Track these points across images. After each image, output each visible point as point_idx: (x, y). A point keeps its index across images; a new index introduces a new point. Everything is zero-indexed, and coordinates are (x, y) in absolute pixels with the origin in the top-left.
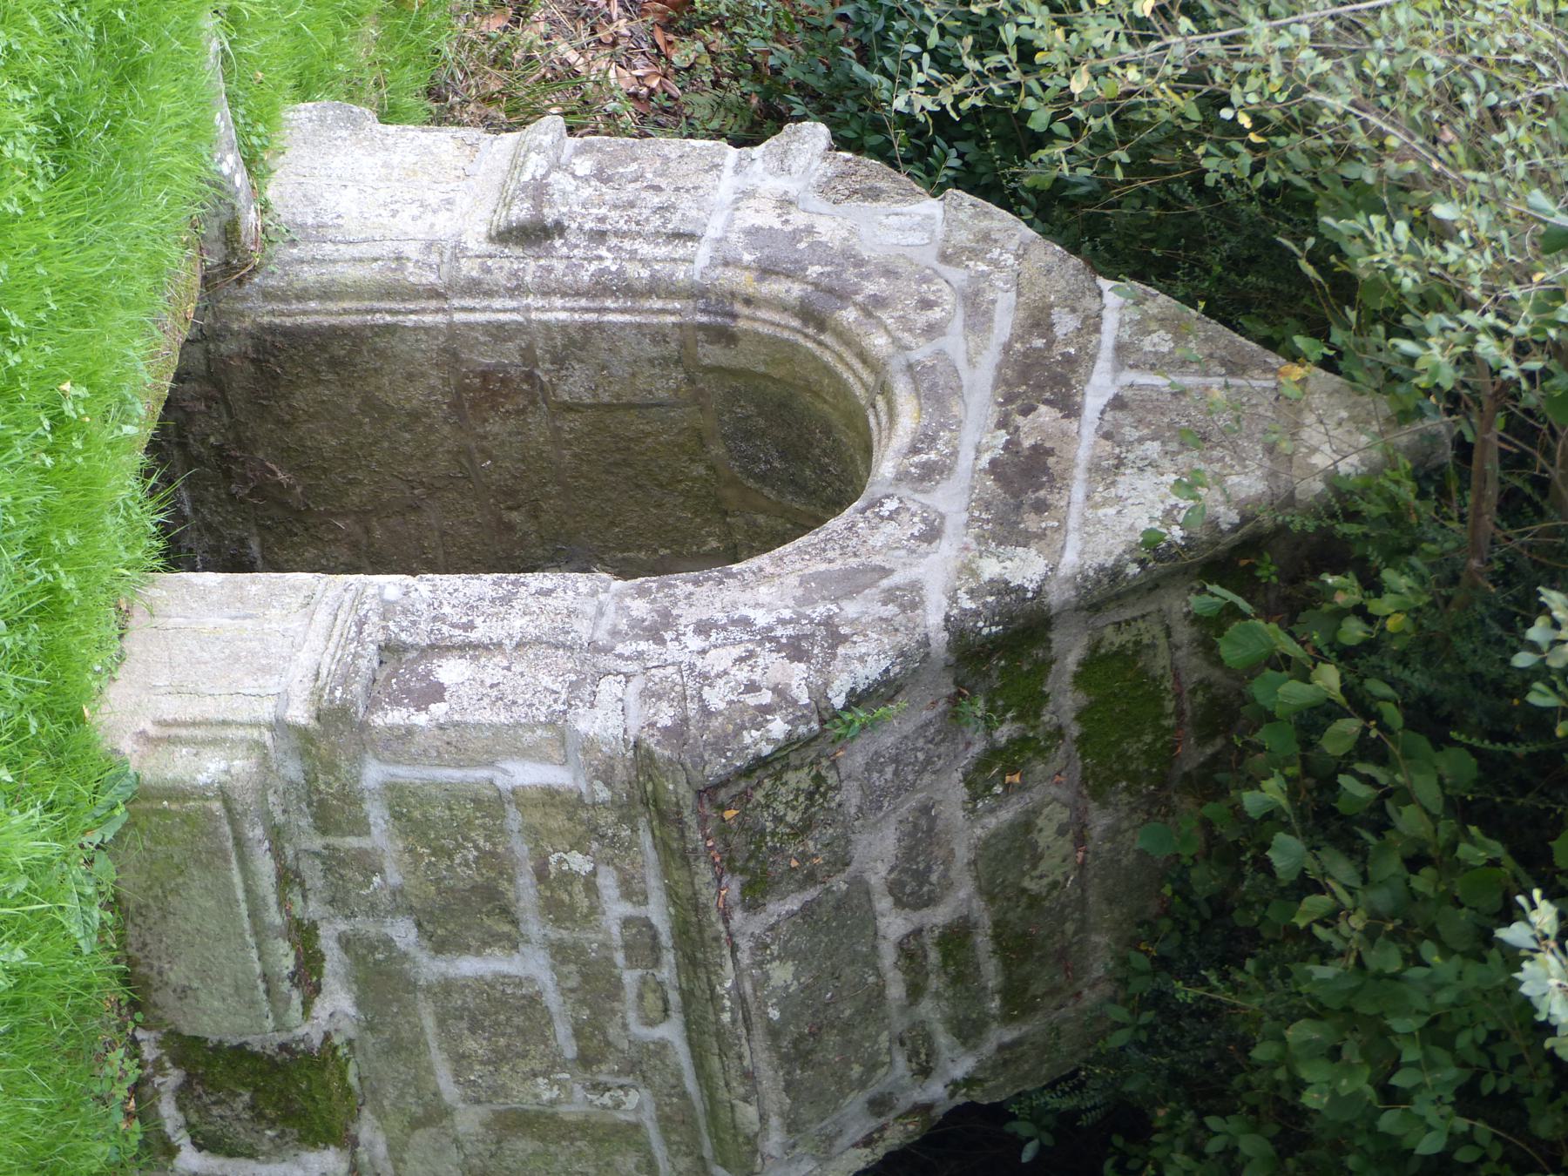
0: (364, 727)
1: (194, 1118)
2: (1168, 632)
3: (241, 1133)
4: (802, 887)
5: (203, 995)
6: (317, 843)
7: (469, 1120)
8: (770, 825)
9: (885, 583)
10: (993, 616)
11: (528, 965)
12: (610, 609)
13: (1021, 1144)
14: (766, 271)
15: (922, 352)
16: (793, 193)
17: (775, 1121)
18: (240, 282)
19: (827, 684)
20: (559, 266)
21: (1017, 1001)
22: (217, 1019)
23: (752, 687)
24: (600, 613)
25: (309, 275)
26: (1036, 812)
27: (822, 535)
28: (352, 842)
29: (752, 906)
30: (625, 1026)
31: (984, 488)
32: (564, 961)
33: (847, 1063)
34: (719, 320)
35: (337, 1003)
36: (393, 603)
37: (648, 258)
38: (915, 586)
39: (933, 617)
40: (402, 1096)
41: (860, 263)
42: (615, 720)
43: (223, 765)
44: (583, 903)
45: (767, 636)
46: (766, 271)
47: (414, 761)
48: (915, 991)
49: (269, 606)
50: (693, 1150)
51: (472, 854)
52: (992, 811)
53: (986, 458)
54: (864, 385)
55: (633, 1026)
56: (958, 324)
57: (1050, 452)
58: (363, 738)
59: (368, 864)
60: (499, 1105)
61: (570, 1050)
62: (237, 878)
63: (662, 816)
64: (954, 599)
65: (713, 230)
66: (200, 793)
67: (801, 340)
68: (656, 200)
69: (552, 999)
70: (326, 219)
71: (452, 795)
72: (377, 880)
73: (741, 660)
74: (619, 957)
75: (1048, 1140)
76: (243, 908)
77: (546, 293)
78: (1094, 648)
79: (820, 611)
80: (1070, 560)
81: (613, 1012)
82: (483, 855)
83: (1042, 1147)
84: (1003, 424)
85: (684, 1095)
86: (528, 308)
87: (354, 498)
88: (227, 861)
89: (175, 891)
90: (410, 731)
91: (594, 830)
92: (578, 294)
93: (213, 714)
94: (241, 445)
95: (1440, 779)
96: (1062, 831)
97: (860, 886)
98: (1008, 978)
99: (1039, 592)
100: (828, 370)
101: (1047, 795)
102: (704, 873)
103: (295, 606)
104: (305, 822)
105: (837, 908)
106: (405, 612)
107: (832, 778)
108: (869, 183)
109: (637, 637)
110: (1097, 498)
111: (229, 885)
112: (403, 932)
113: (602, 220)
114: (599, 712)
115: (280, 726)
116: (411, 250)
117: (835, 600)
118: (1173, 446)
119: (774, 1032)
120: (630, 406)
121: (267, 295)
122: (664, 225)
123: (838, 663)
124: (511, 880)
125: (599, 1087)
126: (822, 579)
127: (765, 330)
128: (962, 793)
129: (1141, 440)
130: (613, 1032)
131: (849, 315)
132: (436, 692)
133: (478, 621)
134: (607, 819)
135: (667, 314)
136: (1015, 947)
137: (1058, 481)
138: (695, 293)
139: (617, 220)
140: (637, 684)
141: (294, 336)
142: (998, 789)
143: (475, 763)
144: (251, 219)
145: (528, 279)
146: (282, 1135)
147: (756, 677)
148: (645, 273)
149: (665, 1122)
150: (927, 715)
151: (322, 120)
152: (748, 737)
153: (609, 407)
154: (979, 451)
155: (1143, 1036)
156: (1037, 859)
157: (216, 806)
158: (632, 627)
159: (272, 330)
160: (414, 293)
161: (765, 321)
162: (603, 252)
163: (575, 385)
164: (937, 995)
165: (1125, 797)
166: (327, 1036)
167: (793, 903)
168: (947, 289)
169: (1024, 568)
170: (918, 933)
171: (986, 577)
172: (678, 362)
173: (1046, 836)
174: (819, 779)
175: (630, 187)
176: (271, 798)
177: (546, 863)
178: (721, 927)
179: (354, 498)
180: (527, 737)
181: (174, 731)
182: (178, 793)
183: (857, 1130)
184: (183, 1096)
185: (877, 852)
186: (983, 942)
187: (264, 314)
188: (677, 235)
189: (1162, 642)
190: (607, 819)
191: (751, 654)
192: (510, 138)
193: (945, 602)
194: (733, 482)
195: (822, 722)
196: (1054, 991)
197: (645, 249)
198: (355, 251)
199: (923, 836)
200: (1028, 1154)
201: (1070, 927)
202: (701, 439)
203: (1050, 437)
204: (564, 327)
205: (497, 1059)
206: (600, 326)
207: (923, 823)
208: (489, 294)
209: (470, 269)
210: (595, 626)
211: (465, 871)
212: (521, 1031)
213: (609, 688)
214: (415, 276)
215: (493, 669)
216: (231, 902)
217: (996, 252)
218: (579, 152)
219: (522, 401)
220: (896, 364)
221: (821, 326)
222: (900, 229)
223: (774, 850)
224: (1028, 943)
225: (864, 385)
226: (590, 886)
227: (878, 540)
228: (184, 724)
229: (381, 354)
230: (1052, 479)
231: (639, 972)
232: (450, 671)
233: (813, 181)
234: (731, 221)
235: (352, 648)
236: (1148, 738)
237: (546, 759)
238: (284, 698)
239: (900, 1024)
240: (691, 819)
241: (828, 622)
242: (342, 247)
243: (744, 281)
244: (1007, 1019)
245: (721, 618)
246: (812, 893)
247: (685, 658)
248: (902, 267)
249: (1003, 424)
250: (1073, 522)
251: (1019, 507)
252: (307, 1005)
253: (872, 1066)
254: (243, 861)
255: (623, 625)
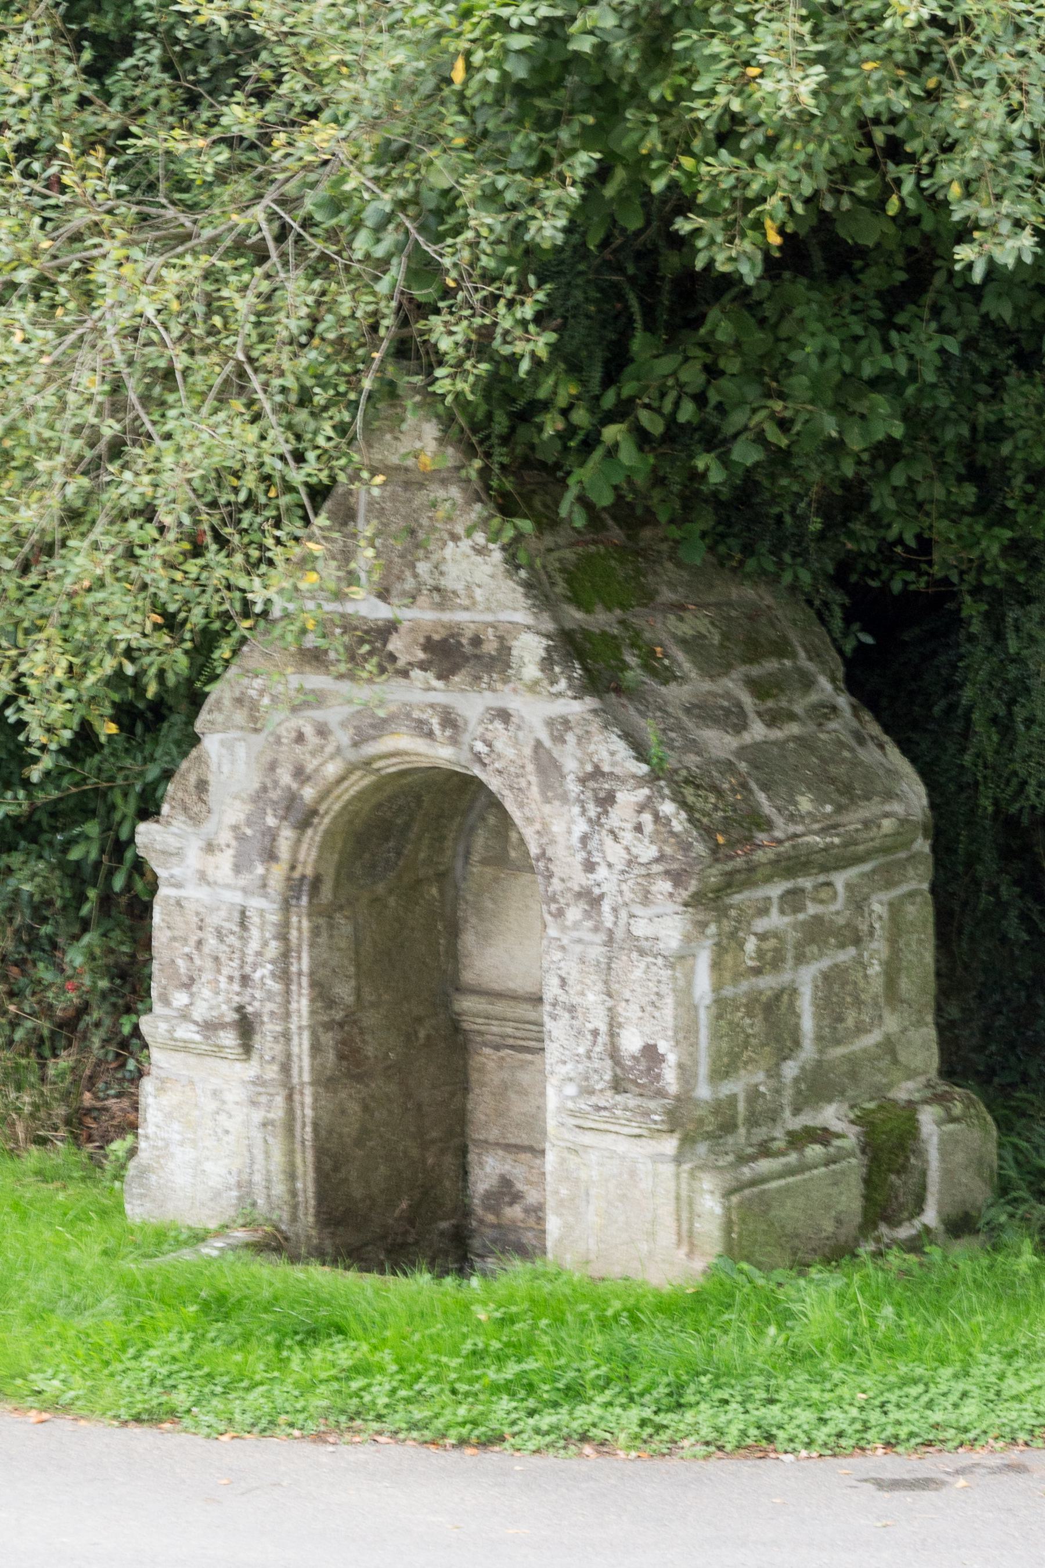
0: (678, 1098)
1: (906, 1214)
2: (550, 550)
3: (913, 1180)
4: (750, 791)
5: (839, 1208)
6: (742, 1131)
7: (892, 1023)
8: (721, 814)
9: (547, 743)
10: (568, 668)
11: (806, 980)
12: (576, 934)
13: (861, 644)
14: (271, 856)
15: (343, 737)
16: (202, 844)
17: (887, 808)
18: (287, 1239)
19: (634, 776)
20: (270, 1006)
21: (782, 649)
22: (850, 1200)
23: (639, 828)
24: (580, 941)
25: (279, 1189)
26: (674, 636)
27: (506, 792)
28: (741, 1106)
29: (767, 825)
30: (838, 913)
31: (463, 682)
32: (804, 955)
33: (844, 760)
34: (300, 888)
35: (831, 1115)
36: (580, 1087)
37: (261, 941)
38: (550, 723)
39: (577, 708)
40: (879, 1070)
41: (264, 789)
42: (668, 921)
43: (708, 1196)
44: (772, 943)
45: (595, 823)
46: (271, 856)
47: (696, 1063)
48: (792, 717)
49: (577, 1180)
50: (902, 865)
51: (748, 1021)
52: (680, 666)
53: (439, 684)
54: (362, 778)
55: (837, 909)
56: (318, 714)
57: (429, 639)
58: (683, 1099)
59: (753, 1095)
60: (882, 1001)
61: (852, 951)
62: (774, 1185)
63: (729, 885)
64: (560, 695)
65: (238, 898)
66: (728, 1210)
67: (322, 828)
68: (212, 942)
69: (825, 964)
70: (233, 1181)
71: (716, 1035)
72: (762, 1089)
73: (616, 838)
74: (801, 917)
75: (856, 626)
76: (791, 1180)
77: (287, 1015)
78: (569, 600)
79: (573, 787)
80: (522, 617)
81: (831, 921)
82: (749, 1014)
83: (862, 630)
84: (405, 674)
85: (874, 871)
86: (300, 1028)
87: (415, 1152)
88: (764, 1192)
89: (783, 1227)
90: (681, 1066)
91: (733, 935)
92: (288, 992)
93: (671, 1207)
94: (384, 1237)
95: (656, 357)
96: (681, 619)
97: (742, 752)
98: (772, 654)
99: (548, 636)
100: (344, 808)
101: (666, 629)
102: (760, 856)
103: (578, 1160)
104: (730, 1140)
105: (757, 768)
106: (587, 1079)
107: (684, 773)
108: (192, 789)
109: (599, 913)
110: (466, 602)
111: (779, 1190)
112: (790, 1070)
113: (231, 978)
114: (662, 934)
115: (678, 1159)
116: (258, 1116)
117: (563, 777)
118: (421, 553)
119: (839, 809)
120: (357, 953)
121: (294, 1219)
122: (232, 933)
123: (617, 770)
124: (761, 993)
125: (871, 933)
126: (545, 787)
127: (314, 854)
128: (673, 686)
129: (416, 576)
130: (841, 921)
131: (309, 793)
132: (651, 1053)
133: (590, 1026)
134: (727, 925)
135: (301, 925)
136: (754, 650)
137: (454, 633)
138: (286, 906)
139: (231, 968)
140: (638, 910)
141: (322, 1196)
142: (666, 662)
143: (696, 1021)
144: (241, 1235)
145: (278, 1028)
146: (913, 1152)
147: (629, 826)
148: (274, 944)
149: (889, 884)
150: (632, 711)
151: (142, 1196)
152: (677, 827)
153: (358, 966)
154: (429, 689)
155: (800, 560)
156: (701, 636)
157: (735, 1199)
158: (590, 917)
159: (317, 1214)
160: (290, 1112)
161: (308, 855)
162: (257, 976)
163: (344, 991)
164: (790, 701)
165: (650, 578)
166: (852, 1122)
167: (762, 797)
168: (287, 724)
169: (530, 649)
170: (759, 714)
171: (539, 674)
172: (330, 917)
173: (685, 629)
174: (687, 782)
175: (198, 962)
176: (721, 1163)
177: (752, 968)
178: (787, 844)
179: (415, 1152)
180: (681, 983)
181: (684, 1234)
182: (728, 1227)
183: (877, 753)
184: (894, 1222)
185: (720, 742)
186: (755, 671)
187: (308, 1218)
188: (243, 924)
189: (556, 554)
190: (727, 925)
191: (612, 832)
192: (156, 1055)
193: (562, 701)
194: (399, 877)
195: (658, 778)
196: (772, 625)
197: (254, 945)
198: (260, 1157)
199: (703, 711)
200: (868, 639)
201: (733, 613)
202: (376, 900)
203: (415, 641)
204: (312, 1001)
205: (858, 1003)
206: (312, 974)
207: (696, 711)
208: (289, 1056)
209: (272, 1072)
210: (592, 943)
211: (755, 1026)
212: (843, 986)
213: (640, 928)
214: (278, 1113)
215: (629, 1012)
216: (787, 1189)
217: (253, 693)
218: (166, 1002)
219: (356, 1030)
220: (352, 755)
221: (314, 812)
222: (233, 762)
223: (735, 811)
224: (747, 642)
225: (362, 778)
226: (762, 937)
227: (510, 753)
228: (679, 1226)
229: (330, 1132)
230: (452, 636)
231: (809, 904)
232: (631, 1042)
233: (190, 830)
234: (227, 886)
235: (618, 1112)
236: (613, 563)
237: (692, 970)
238: (657, 1158)
239: (812, 727)
240: (729, 867)
241: (583, 781)
242: (256, 1167)
243: (278, 872)
244: (794, 656)
245: (581, 855)
246: (754, 786)
247: (615, 878)
248: (268, 758)
249: (405, 674)
250: (489, 618)
251: (477, 657)
252: (839, 1136)
253: (841, 744)
254: (763, 1180)
255: (589, 924)
